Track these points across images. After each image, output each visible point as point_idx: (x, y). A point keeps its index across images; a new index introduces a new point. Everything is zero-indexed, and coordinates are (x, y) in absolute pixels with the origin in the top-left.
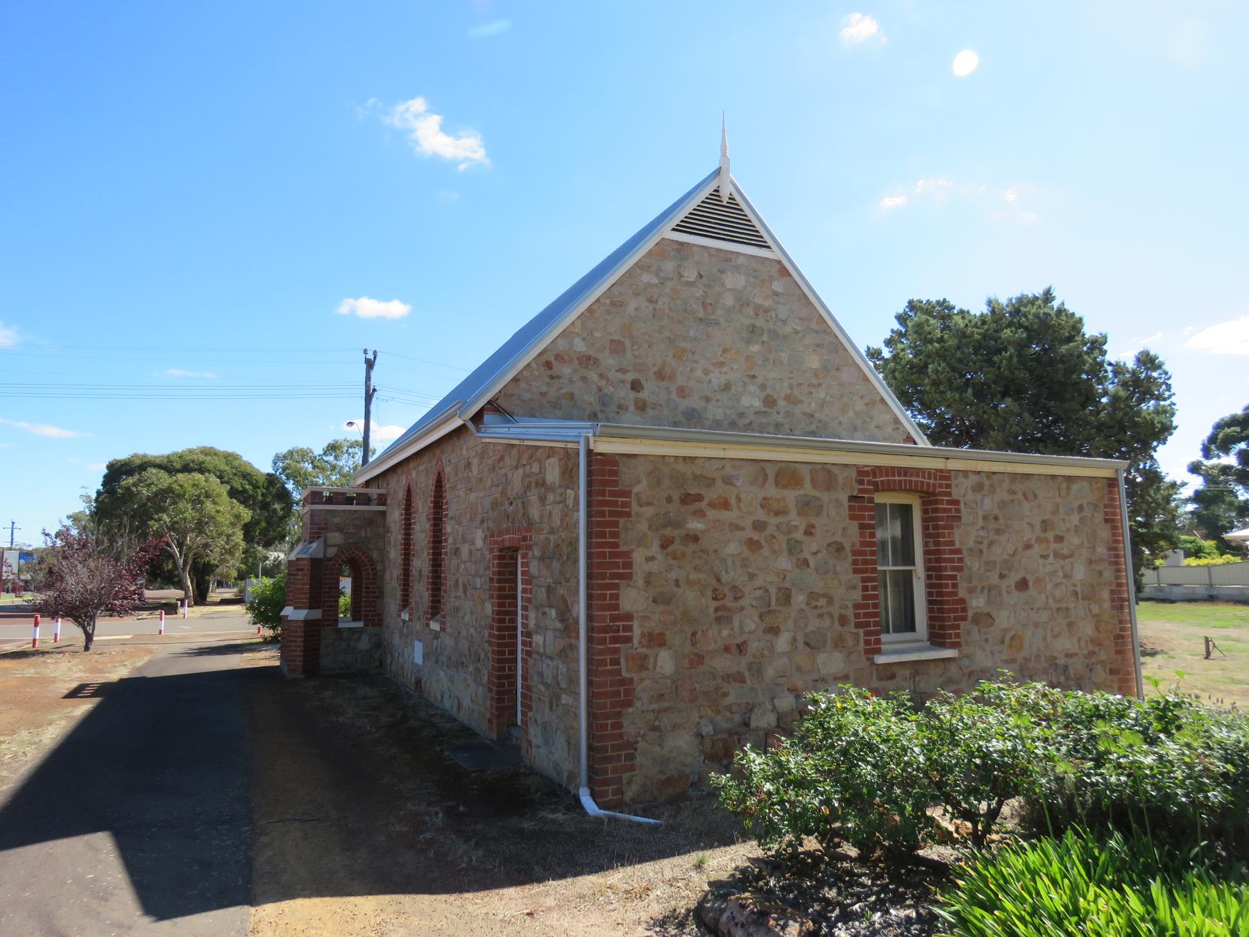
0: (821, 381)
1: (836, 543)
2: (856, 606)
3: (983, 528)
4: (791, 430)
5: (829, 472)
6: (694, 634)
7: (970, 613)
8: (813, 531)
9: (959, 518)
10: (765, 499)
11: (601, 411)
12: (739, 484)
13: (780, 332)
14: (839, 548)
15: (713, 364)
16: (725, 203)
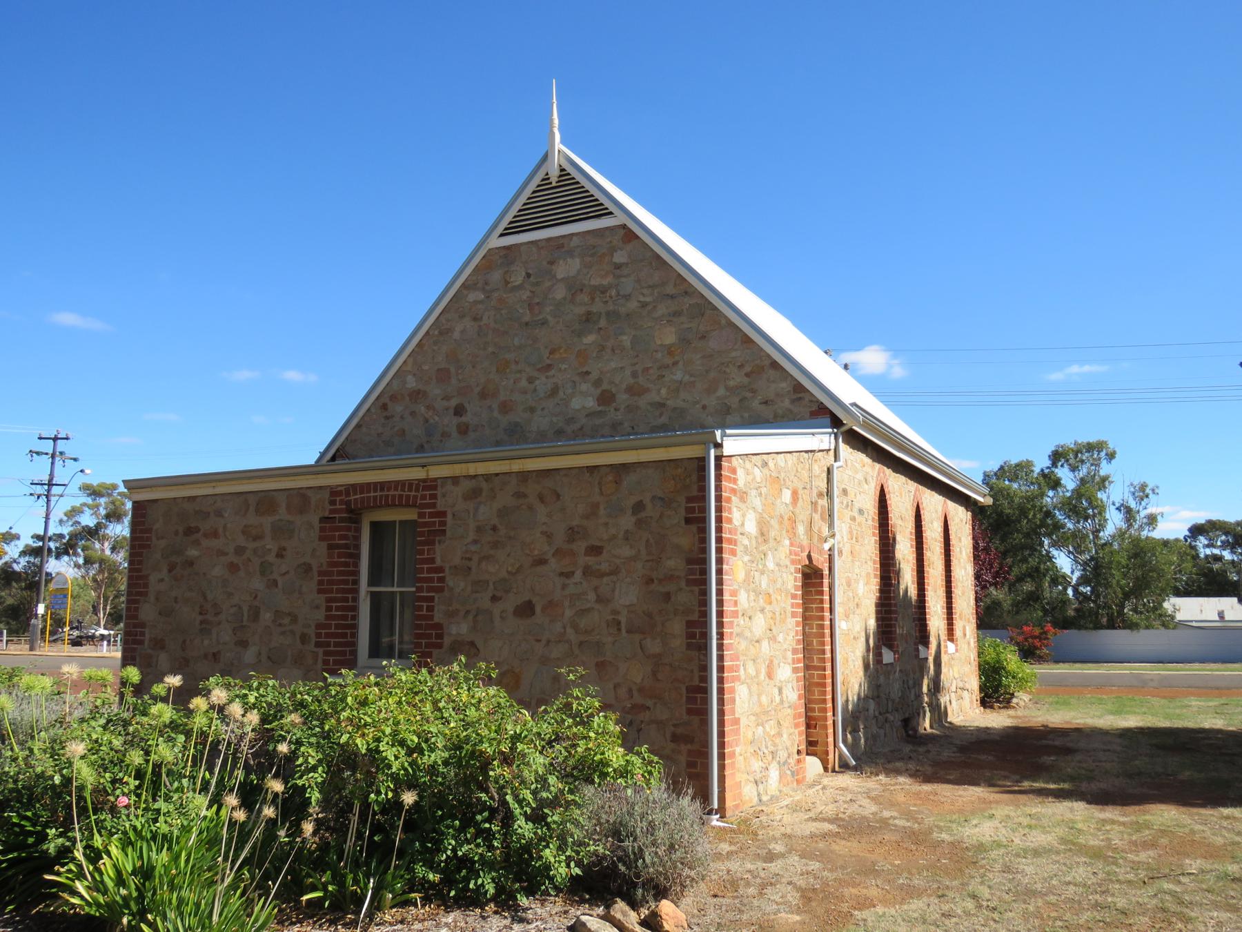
0: (677, 358)
2: (319, 626)
3: (475, 542)
4: (633, 428)
6: (184, 642)
7: (447, 641)
8: (284, 553)
9: (444, 531)
10: (245, 526)
12: (226, 515)
13: (623, 310)
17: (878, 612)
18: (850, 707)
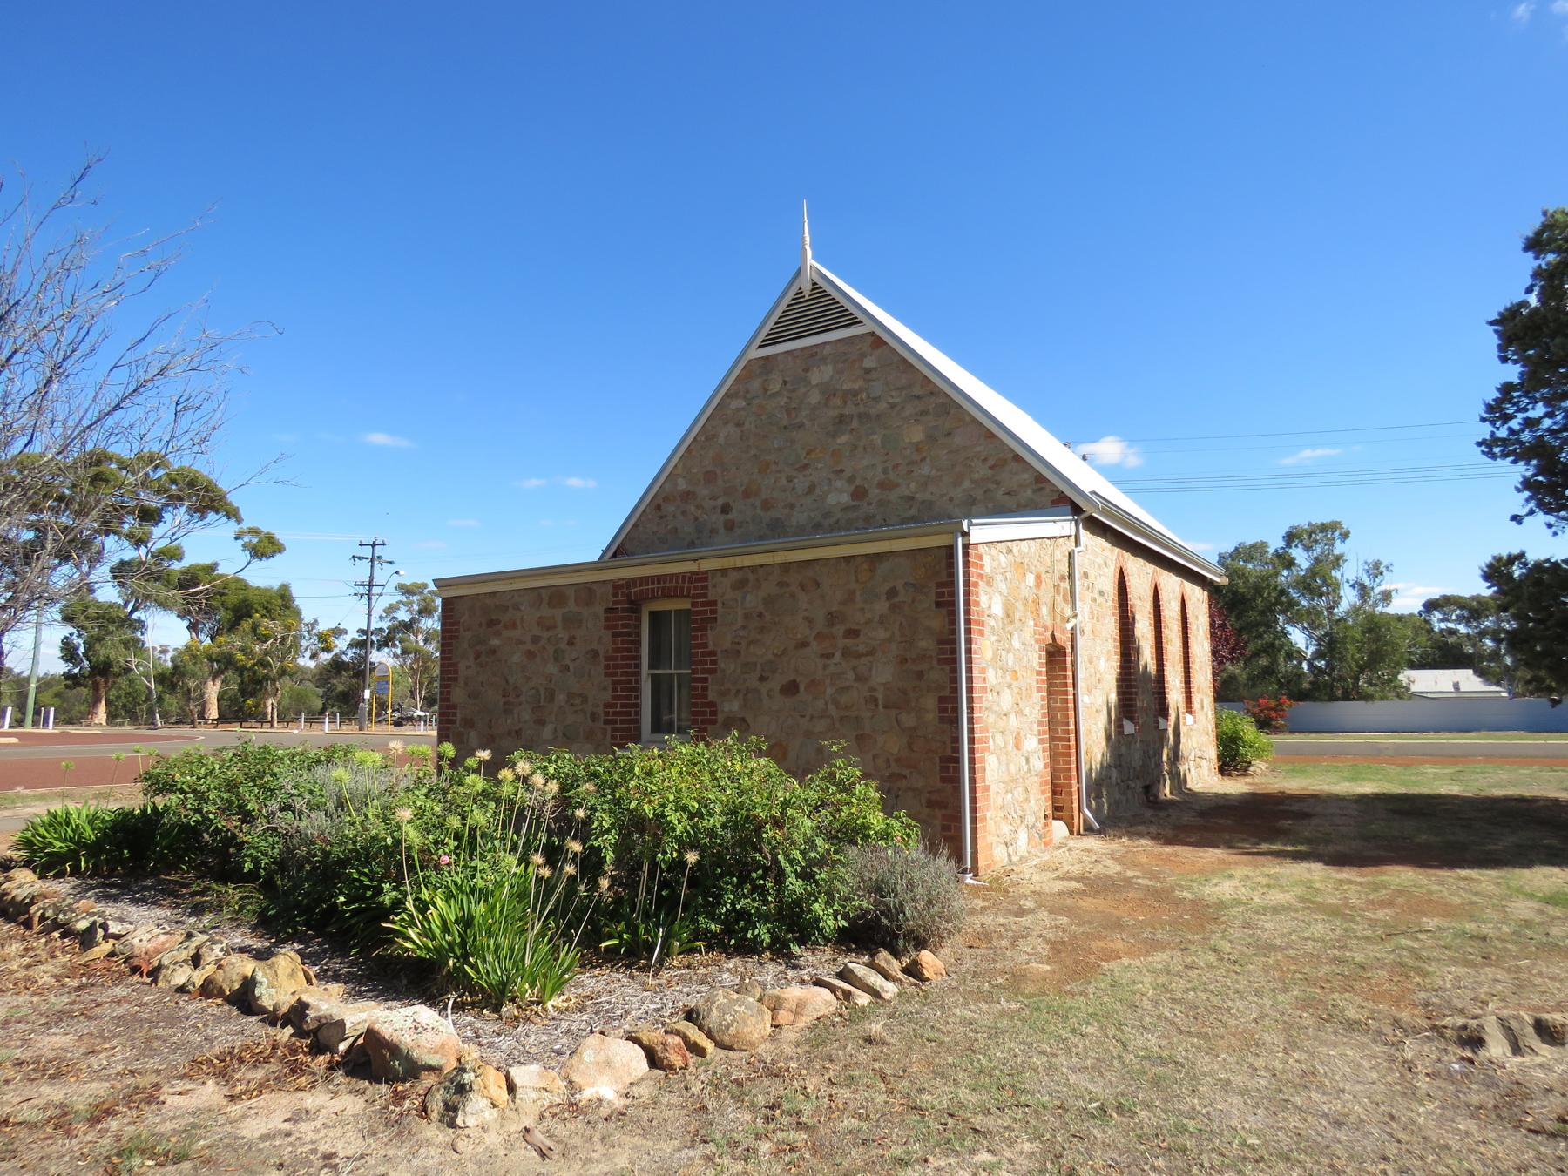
0: (924, 454)
1: (593, 650)
2: (607, 705)
3: (743, 627)
5: (590, 589)
7: (720, 718)
11: (698, 538)
12: (523, 608)
13: (873, 412)
14: (595, 654)
15: (796, 469)
16: (807, 298)
17: (1118, 687)
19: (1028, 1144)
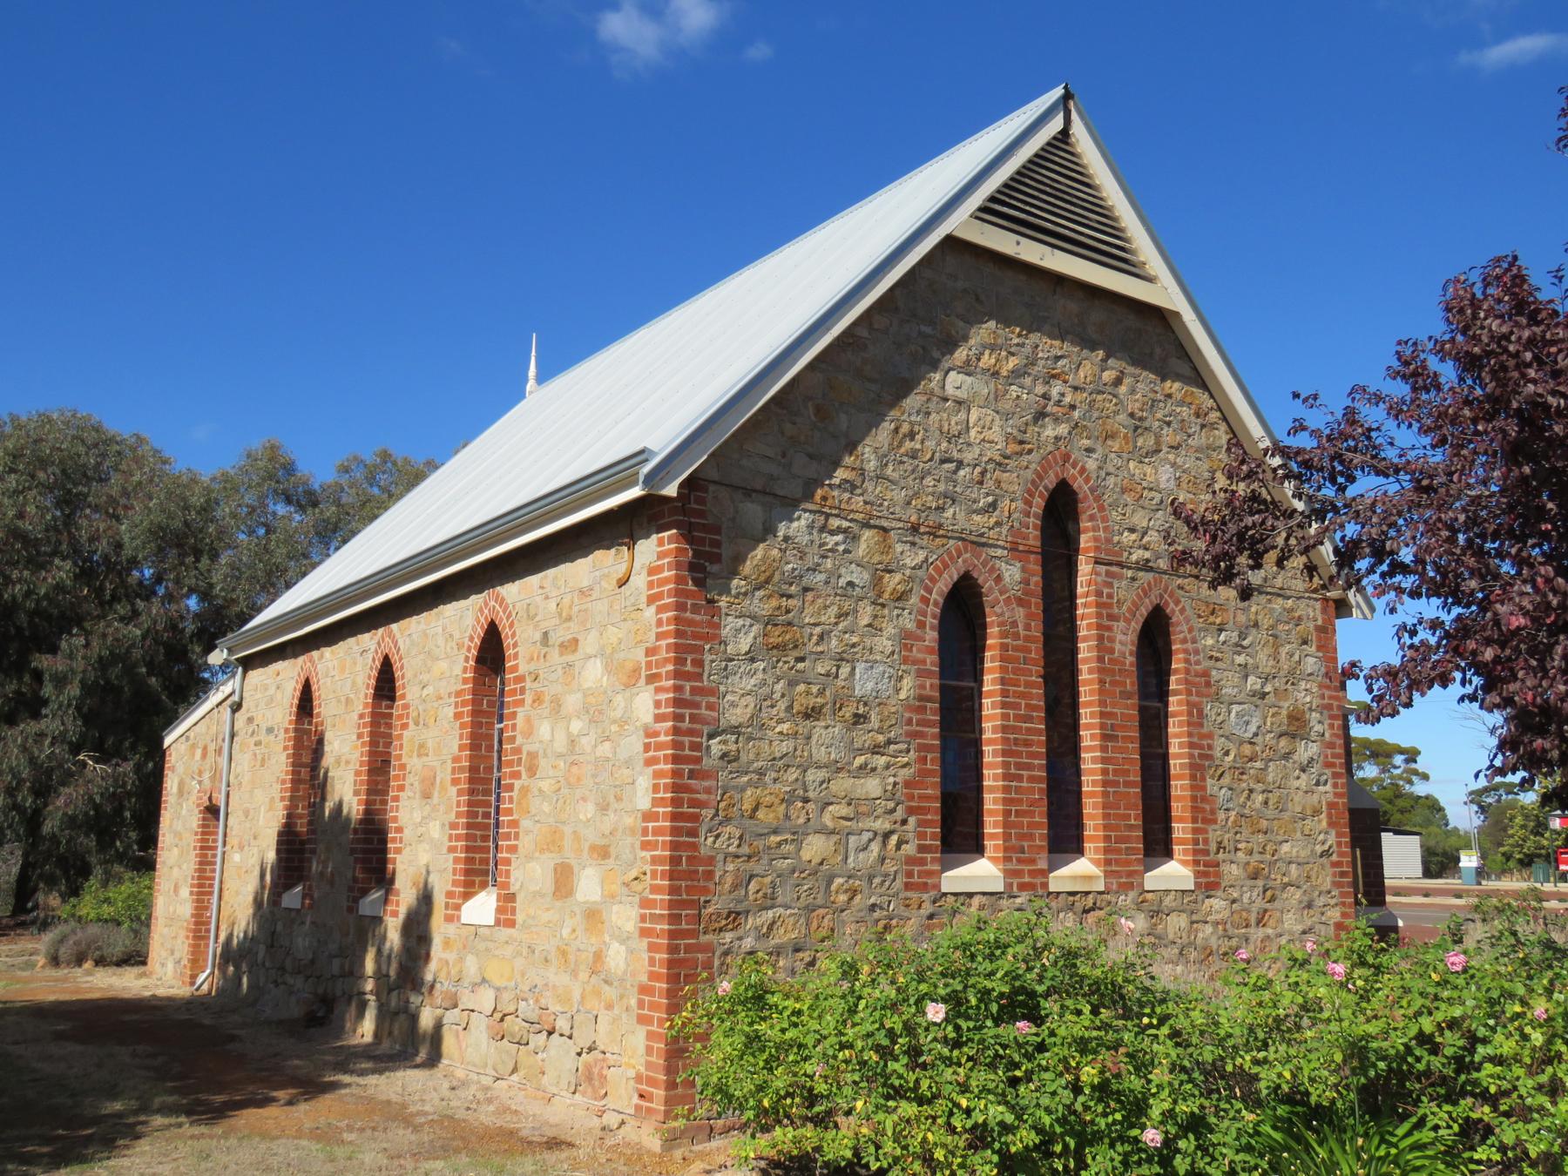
17: (279, 843)
18: (235, 941)
19: (1533, 1037)
